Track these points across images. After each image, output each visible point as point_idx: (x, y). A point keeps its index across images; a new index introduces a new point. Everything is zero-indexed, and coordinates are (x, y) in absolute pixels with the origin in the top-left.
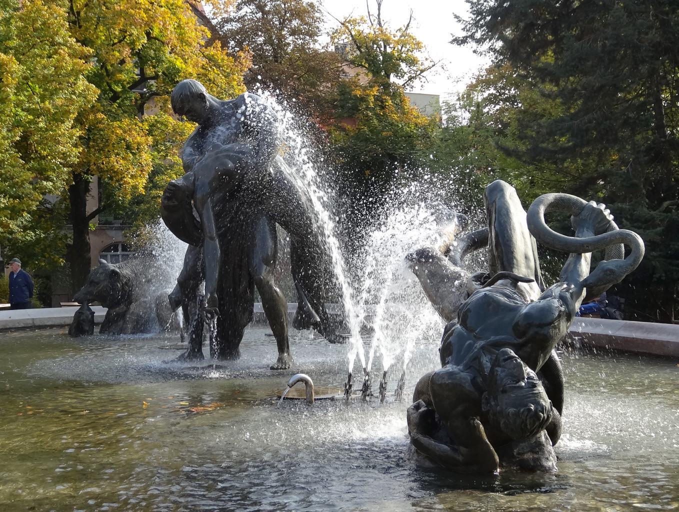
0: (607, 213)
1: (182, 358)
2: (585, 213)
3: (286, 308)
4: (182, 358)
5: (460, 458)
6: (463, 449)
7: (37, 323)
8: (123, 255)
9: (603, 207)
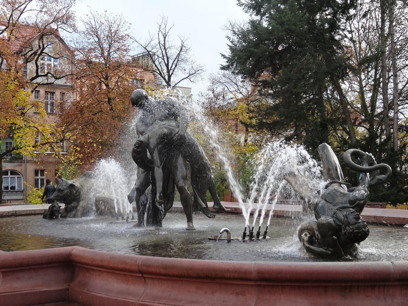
0: (373, 157)
1: (135, 226)
2: (365, 157)
3: (281, 220)
4: (135, 226)
5: (330, 252)
6: (331, 249)
7: (18, 213)
8: (11, 178)
9: (371, 154)
